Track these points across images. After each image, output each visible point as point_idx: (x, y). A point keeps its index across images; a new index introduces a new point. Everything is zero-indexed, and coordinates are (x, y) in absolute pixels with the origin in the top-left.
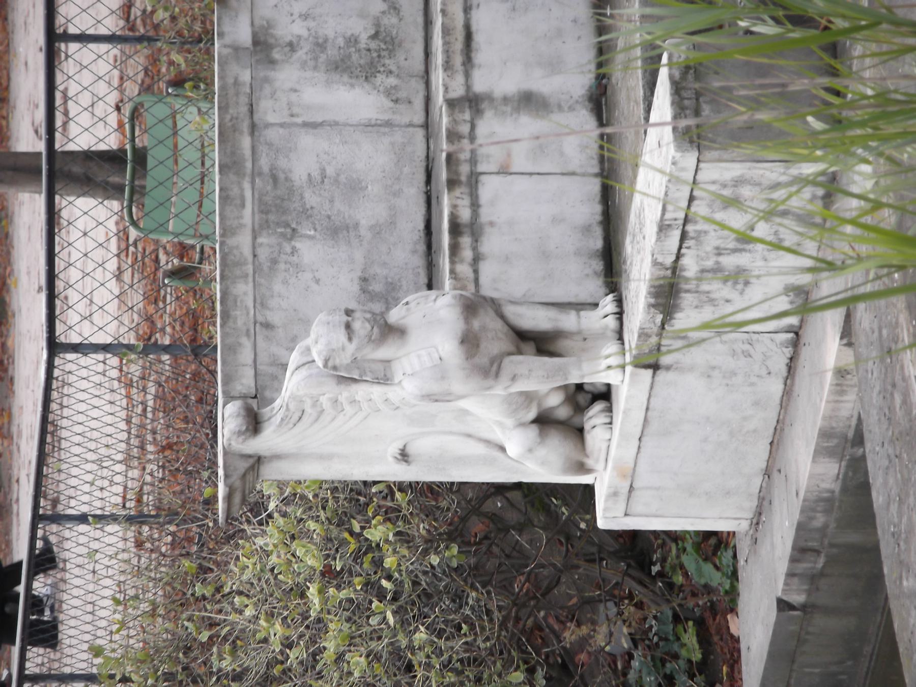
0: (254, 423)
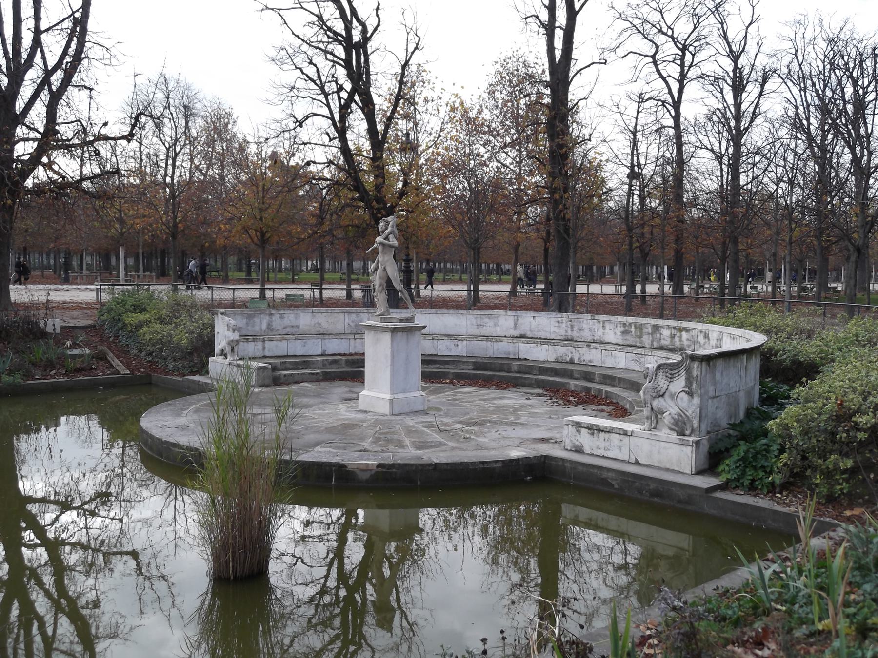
0: (222, 314)
